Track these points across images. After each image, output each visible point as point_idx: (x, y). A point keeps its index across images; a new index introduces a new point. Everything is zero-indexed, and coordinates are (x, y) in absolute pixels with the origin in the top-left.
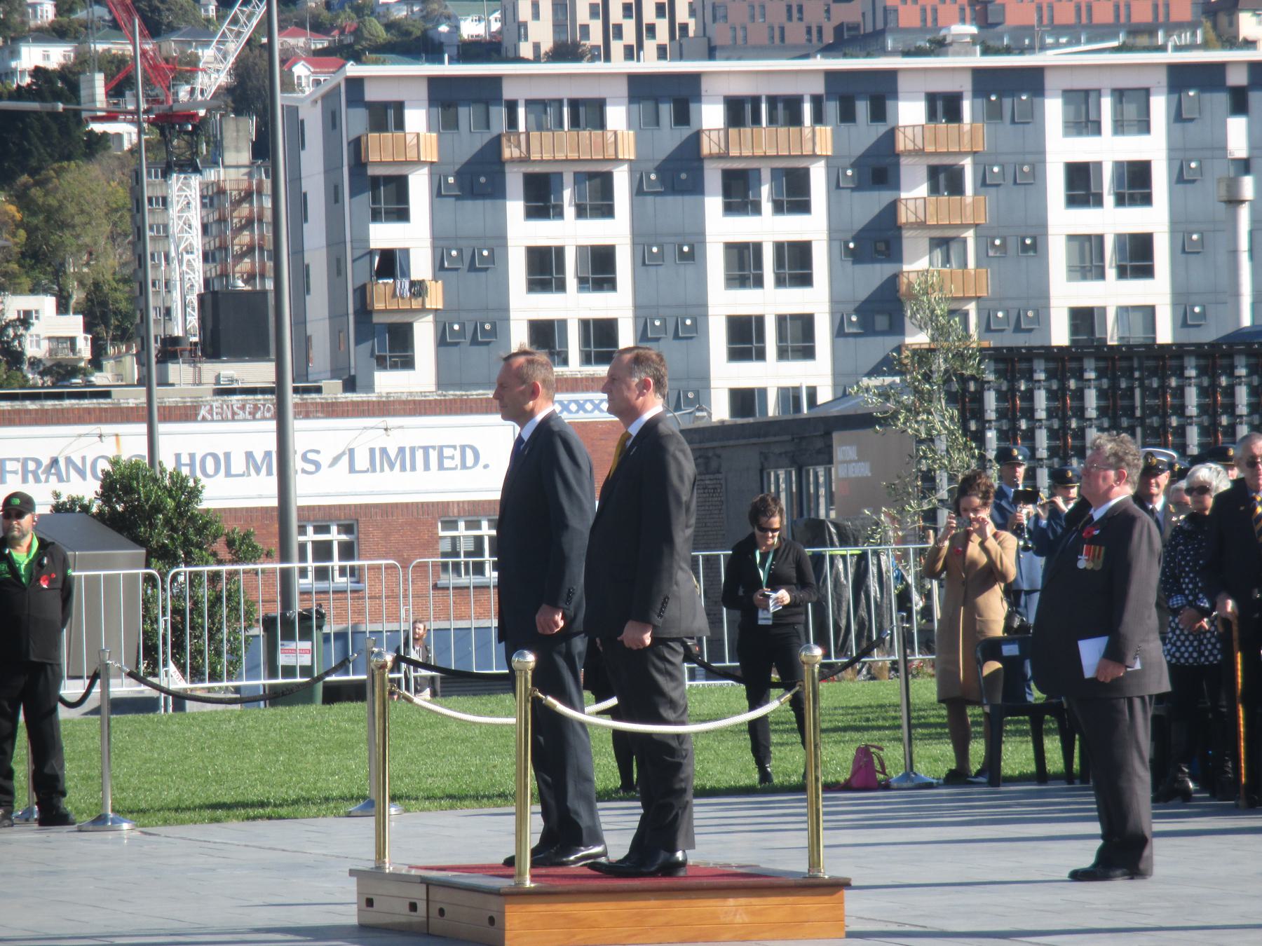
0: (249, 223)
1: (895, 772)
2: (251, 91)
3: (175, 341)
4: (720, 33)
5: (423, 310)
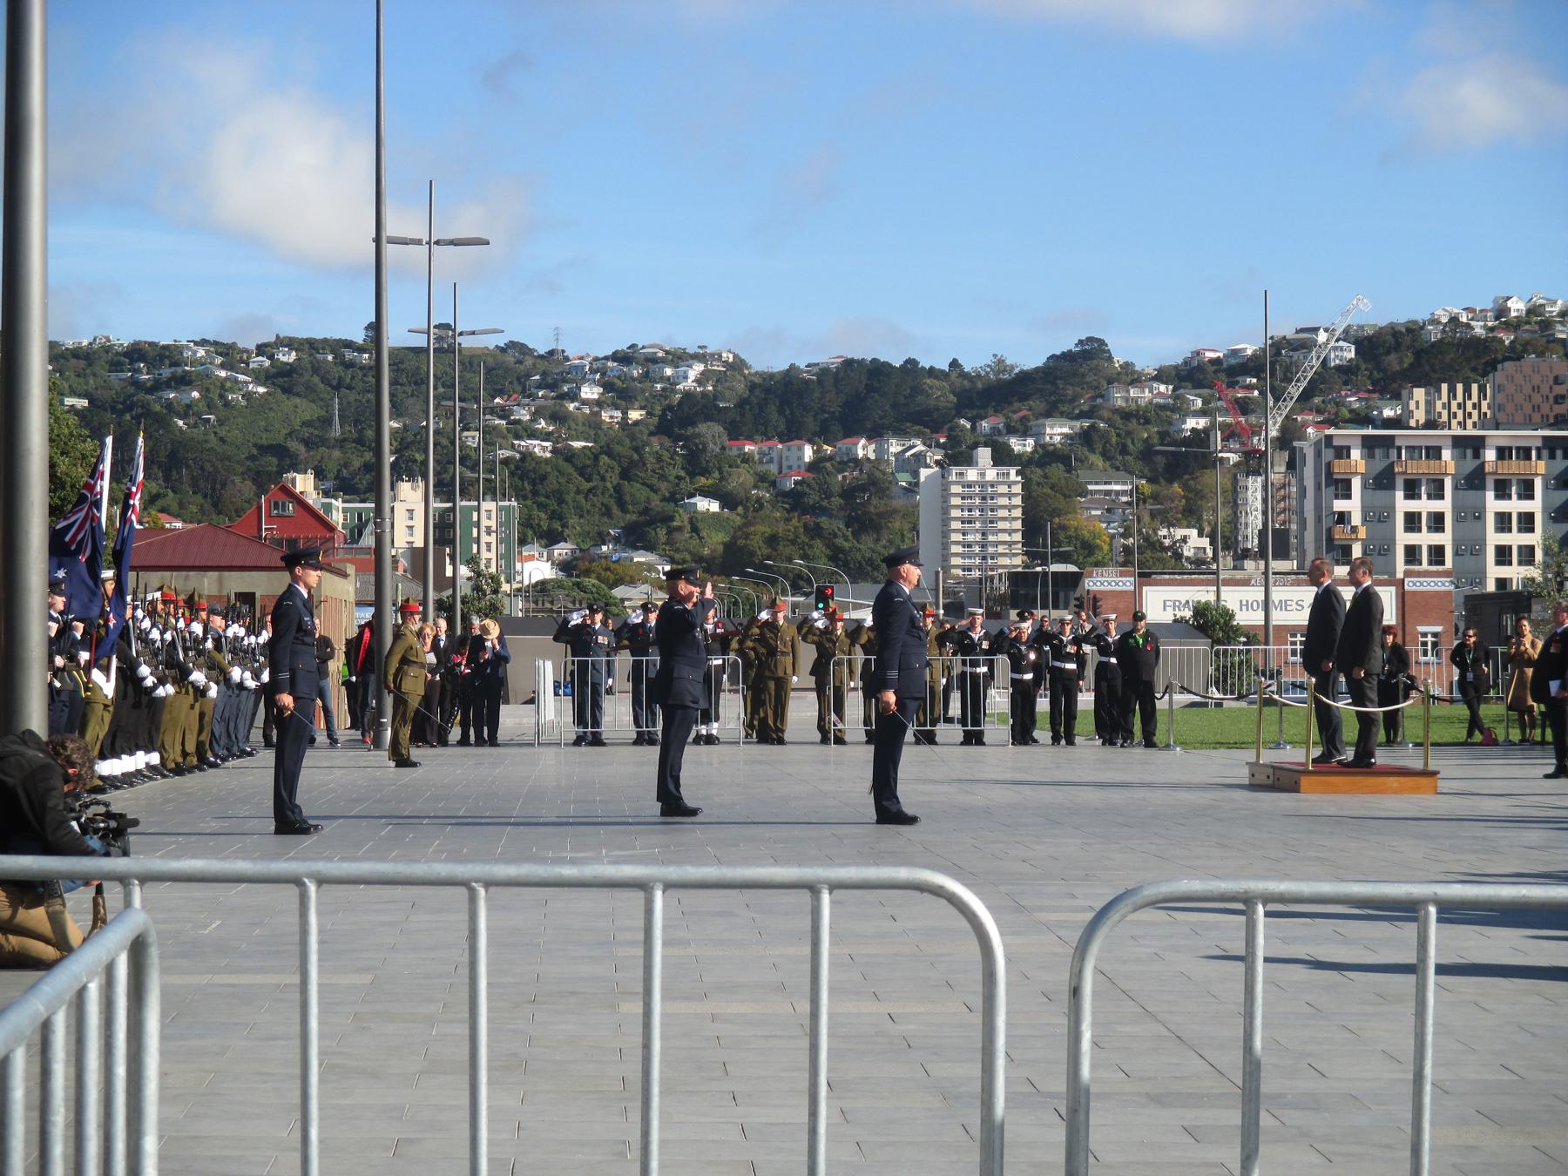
0: (1284, 498)
1: (1501, 738)
2: (1287, 439)
3: (1247, 550)
4: (1501, 417)
5: (1357, 539)
